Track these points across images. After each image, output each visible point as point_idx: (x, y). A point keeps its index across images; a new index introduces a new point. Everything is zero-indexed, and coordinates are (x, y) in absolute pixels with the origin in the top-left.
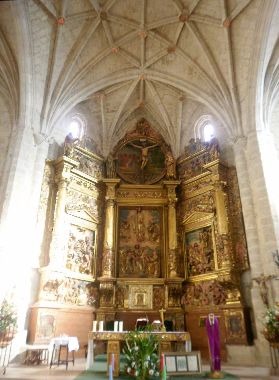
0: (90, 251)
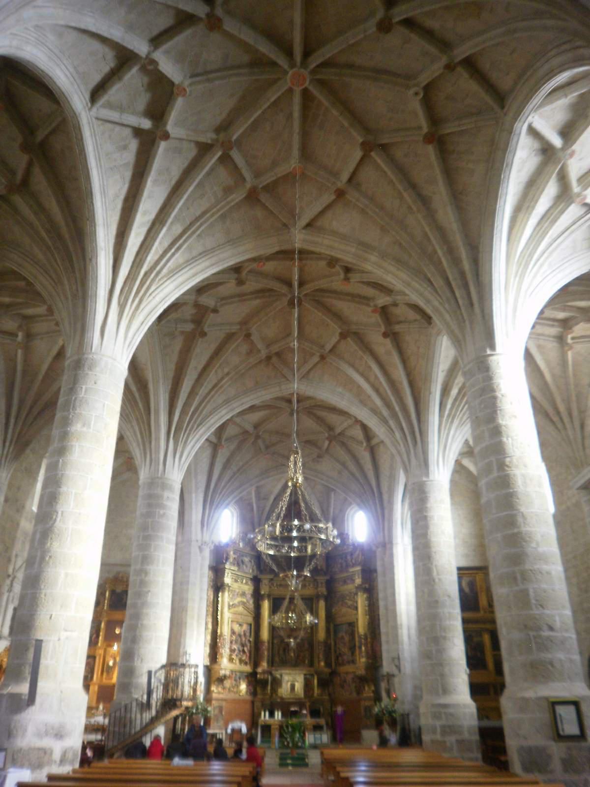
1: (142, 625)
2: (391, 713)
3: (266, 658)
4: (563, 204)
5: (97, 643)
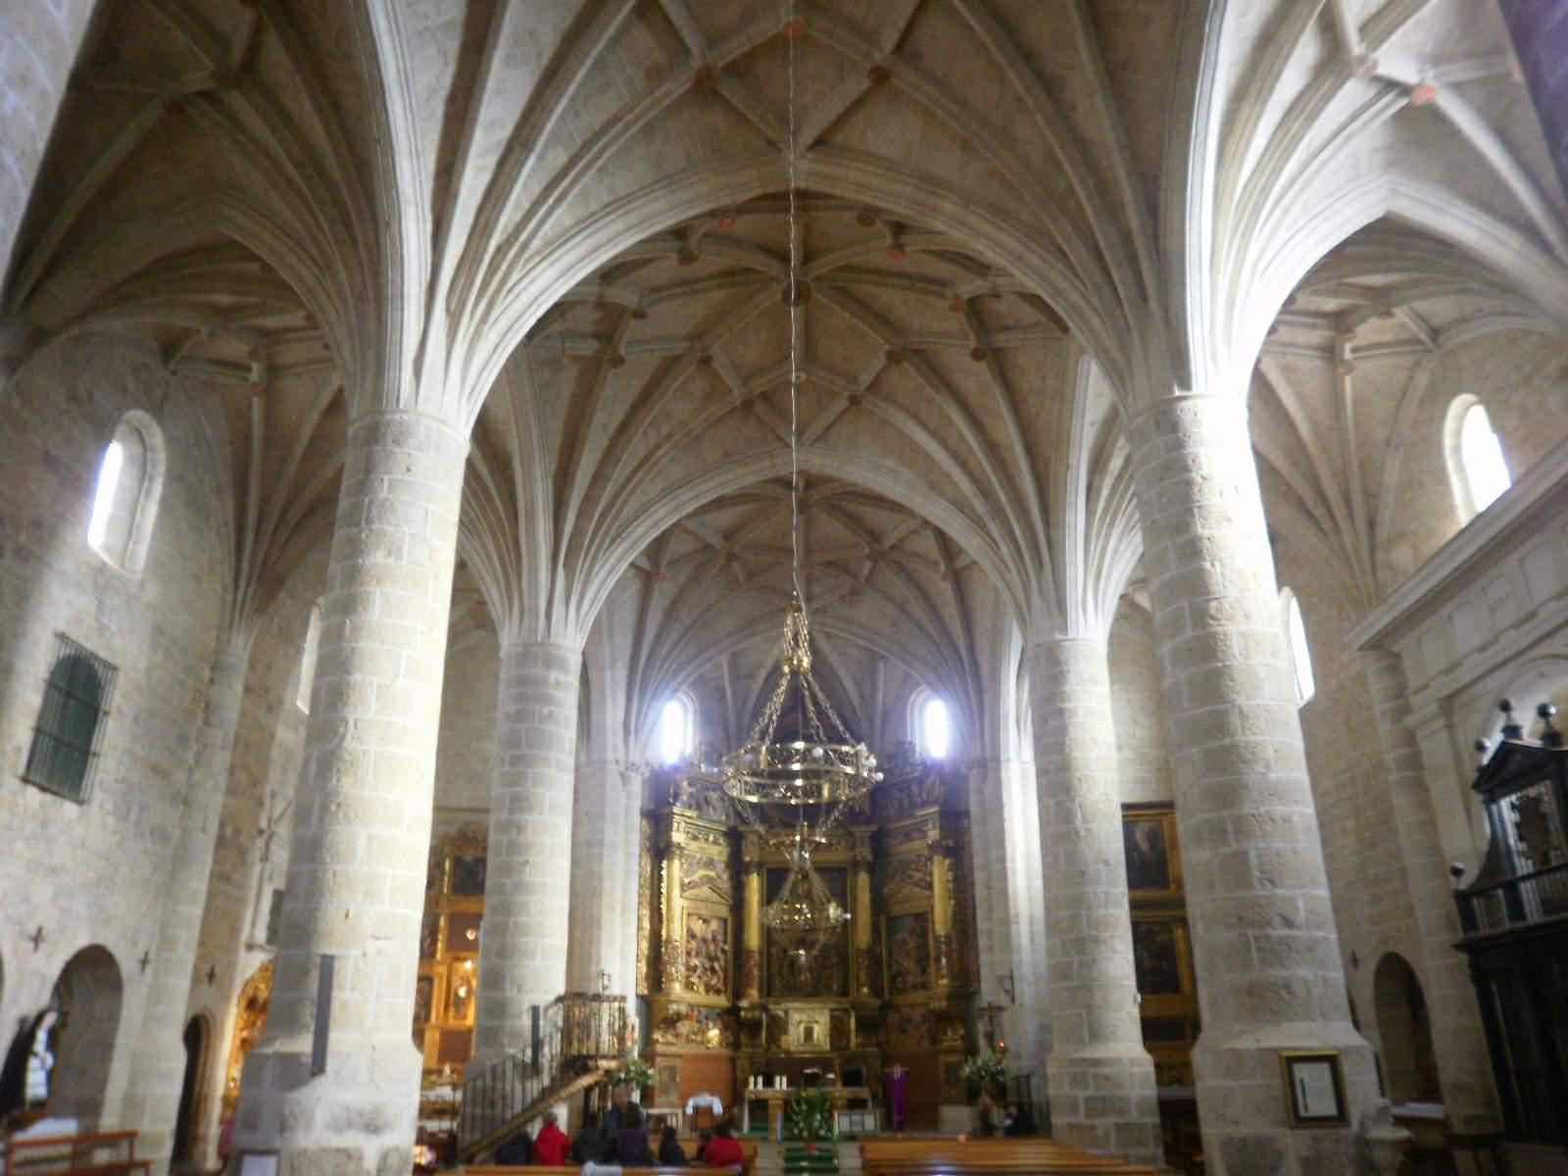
0: (720, 955)
2: (993, 1075)
3: (756, 982)
4: (1328, 84)
5: (432, 954)
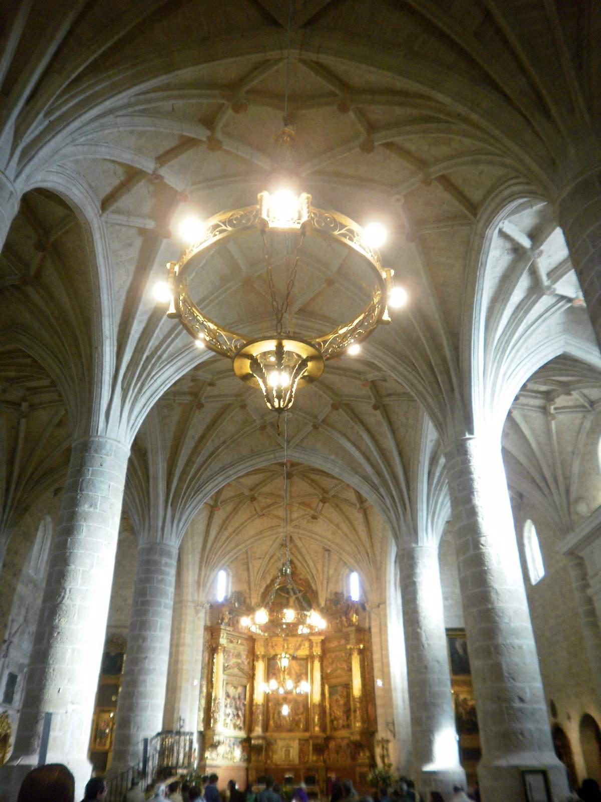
0: (243, 708)
1: (138, 692)
4: (535, 296)
